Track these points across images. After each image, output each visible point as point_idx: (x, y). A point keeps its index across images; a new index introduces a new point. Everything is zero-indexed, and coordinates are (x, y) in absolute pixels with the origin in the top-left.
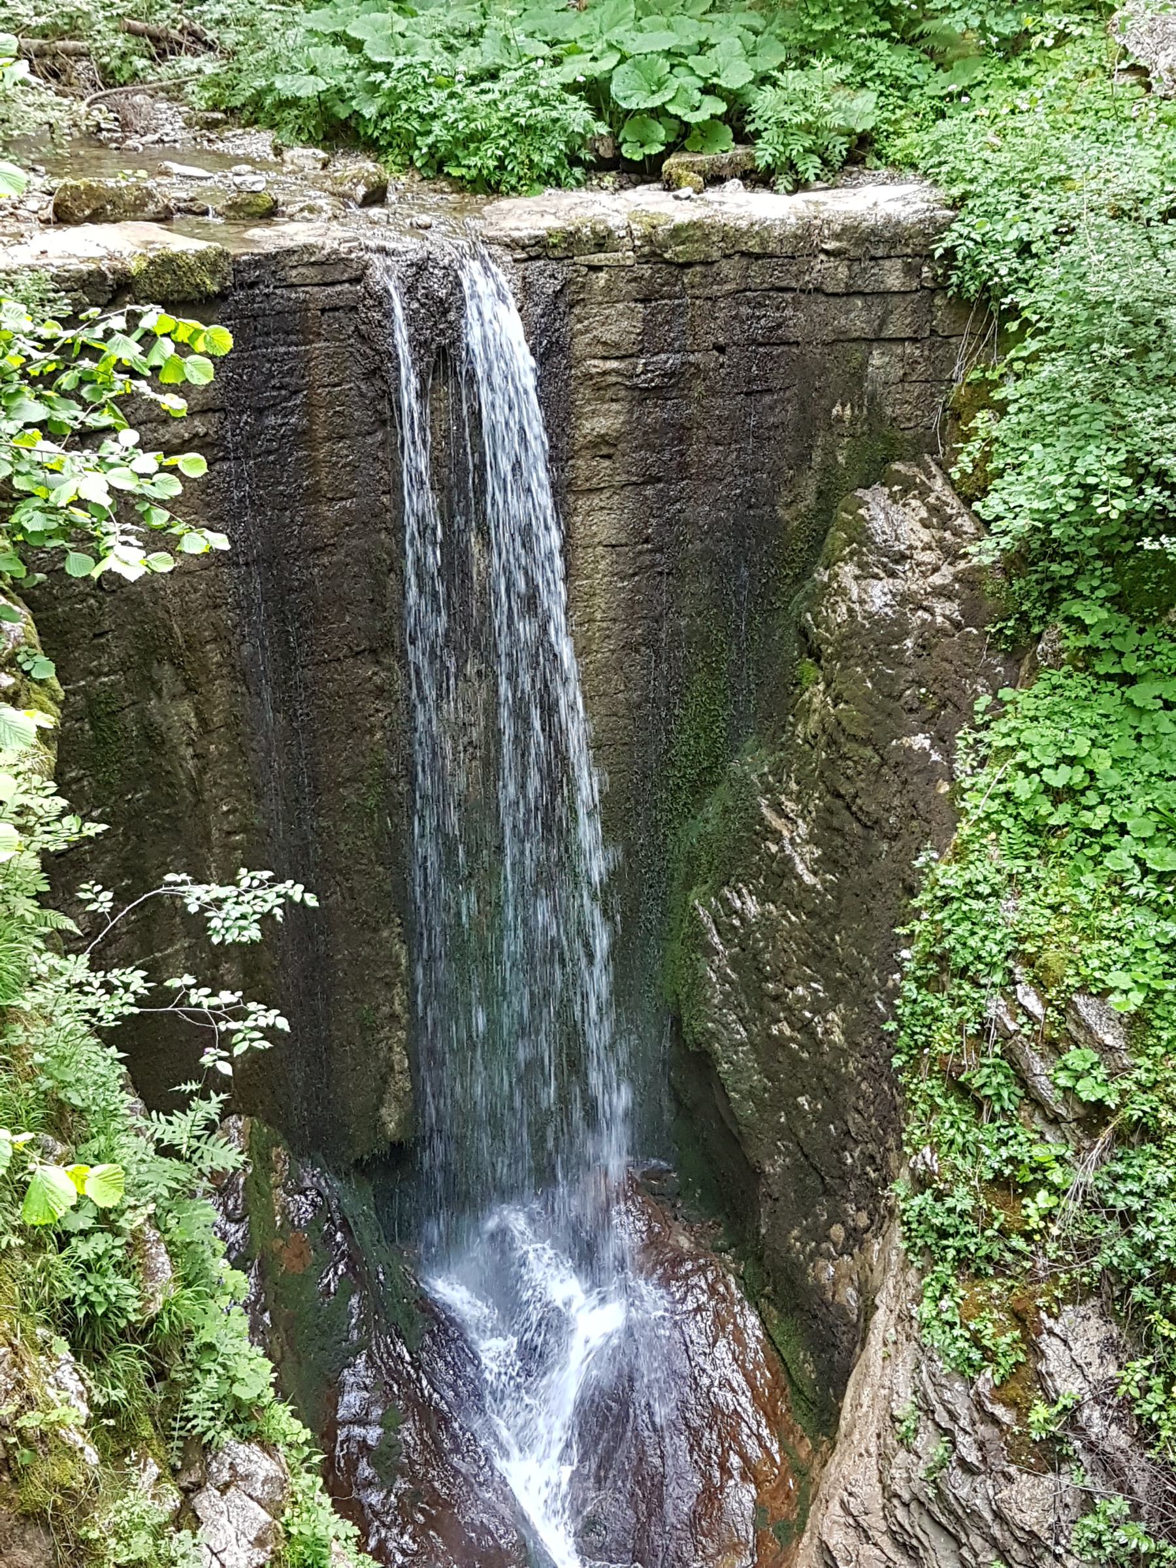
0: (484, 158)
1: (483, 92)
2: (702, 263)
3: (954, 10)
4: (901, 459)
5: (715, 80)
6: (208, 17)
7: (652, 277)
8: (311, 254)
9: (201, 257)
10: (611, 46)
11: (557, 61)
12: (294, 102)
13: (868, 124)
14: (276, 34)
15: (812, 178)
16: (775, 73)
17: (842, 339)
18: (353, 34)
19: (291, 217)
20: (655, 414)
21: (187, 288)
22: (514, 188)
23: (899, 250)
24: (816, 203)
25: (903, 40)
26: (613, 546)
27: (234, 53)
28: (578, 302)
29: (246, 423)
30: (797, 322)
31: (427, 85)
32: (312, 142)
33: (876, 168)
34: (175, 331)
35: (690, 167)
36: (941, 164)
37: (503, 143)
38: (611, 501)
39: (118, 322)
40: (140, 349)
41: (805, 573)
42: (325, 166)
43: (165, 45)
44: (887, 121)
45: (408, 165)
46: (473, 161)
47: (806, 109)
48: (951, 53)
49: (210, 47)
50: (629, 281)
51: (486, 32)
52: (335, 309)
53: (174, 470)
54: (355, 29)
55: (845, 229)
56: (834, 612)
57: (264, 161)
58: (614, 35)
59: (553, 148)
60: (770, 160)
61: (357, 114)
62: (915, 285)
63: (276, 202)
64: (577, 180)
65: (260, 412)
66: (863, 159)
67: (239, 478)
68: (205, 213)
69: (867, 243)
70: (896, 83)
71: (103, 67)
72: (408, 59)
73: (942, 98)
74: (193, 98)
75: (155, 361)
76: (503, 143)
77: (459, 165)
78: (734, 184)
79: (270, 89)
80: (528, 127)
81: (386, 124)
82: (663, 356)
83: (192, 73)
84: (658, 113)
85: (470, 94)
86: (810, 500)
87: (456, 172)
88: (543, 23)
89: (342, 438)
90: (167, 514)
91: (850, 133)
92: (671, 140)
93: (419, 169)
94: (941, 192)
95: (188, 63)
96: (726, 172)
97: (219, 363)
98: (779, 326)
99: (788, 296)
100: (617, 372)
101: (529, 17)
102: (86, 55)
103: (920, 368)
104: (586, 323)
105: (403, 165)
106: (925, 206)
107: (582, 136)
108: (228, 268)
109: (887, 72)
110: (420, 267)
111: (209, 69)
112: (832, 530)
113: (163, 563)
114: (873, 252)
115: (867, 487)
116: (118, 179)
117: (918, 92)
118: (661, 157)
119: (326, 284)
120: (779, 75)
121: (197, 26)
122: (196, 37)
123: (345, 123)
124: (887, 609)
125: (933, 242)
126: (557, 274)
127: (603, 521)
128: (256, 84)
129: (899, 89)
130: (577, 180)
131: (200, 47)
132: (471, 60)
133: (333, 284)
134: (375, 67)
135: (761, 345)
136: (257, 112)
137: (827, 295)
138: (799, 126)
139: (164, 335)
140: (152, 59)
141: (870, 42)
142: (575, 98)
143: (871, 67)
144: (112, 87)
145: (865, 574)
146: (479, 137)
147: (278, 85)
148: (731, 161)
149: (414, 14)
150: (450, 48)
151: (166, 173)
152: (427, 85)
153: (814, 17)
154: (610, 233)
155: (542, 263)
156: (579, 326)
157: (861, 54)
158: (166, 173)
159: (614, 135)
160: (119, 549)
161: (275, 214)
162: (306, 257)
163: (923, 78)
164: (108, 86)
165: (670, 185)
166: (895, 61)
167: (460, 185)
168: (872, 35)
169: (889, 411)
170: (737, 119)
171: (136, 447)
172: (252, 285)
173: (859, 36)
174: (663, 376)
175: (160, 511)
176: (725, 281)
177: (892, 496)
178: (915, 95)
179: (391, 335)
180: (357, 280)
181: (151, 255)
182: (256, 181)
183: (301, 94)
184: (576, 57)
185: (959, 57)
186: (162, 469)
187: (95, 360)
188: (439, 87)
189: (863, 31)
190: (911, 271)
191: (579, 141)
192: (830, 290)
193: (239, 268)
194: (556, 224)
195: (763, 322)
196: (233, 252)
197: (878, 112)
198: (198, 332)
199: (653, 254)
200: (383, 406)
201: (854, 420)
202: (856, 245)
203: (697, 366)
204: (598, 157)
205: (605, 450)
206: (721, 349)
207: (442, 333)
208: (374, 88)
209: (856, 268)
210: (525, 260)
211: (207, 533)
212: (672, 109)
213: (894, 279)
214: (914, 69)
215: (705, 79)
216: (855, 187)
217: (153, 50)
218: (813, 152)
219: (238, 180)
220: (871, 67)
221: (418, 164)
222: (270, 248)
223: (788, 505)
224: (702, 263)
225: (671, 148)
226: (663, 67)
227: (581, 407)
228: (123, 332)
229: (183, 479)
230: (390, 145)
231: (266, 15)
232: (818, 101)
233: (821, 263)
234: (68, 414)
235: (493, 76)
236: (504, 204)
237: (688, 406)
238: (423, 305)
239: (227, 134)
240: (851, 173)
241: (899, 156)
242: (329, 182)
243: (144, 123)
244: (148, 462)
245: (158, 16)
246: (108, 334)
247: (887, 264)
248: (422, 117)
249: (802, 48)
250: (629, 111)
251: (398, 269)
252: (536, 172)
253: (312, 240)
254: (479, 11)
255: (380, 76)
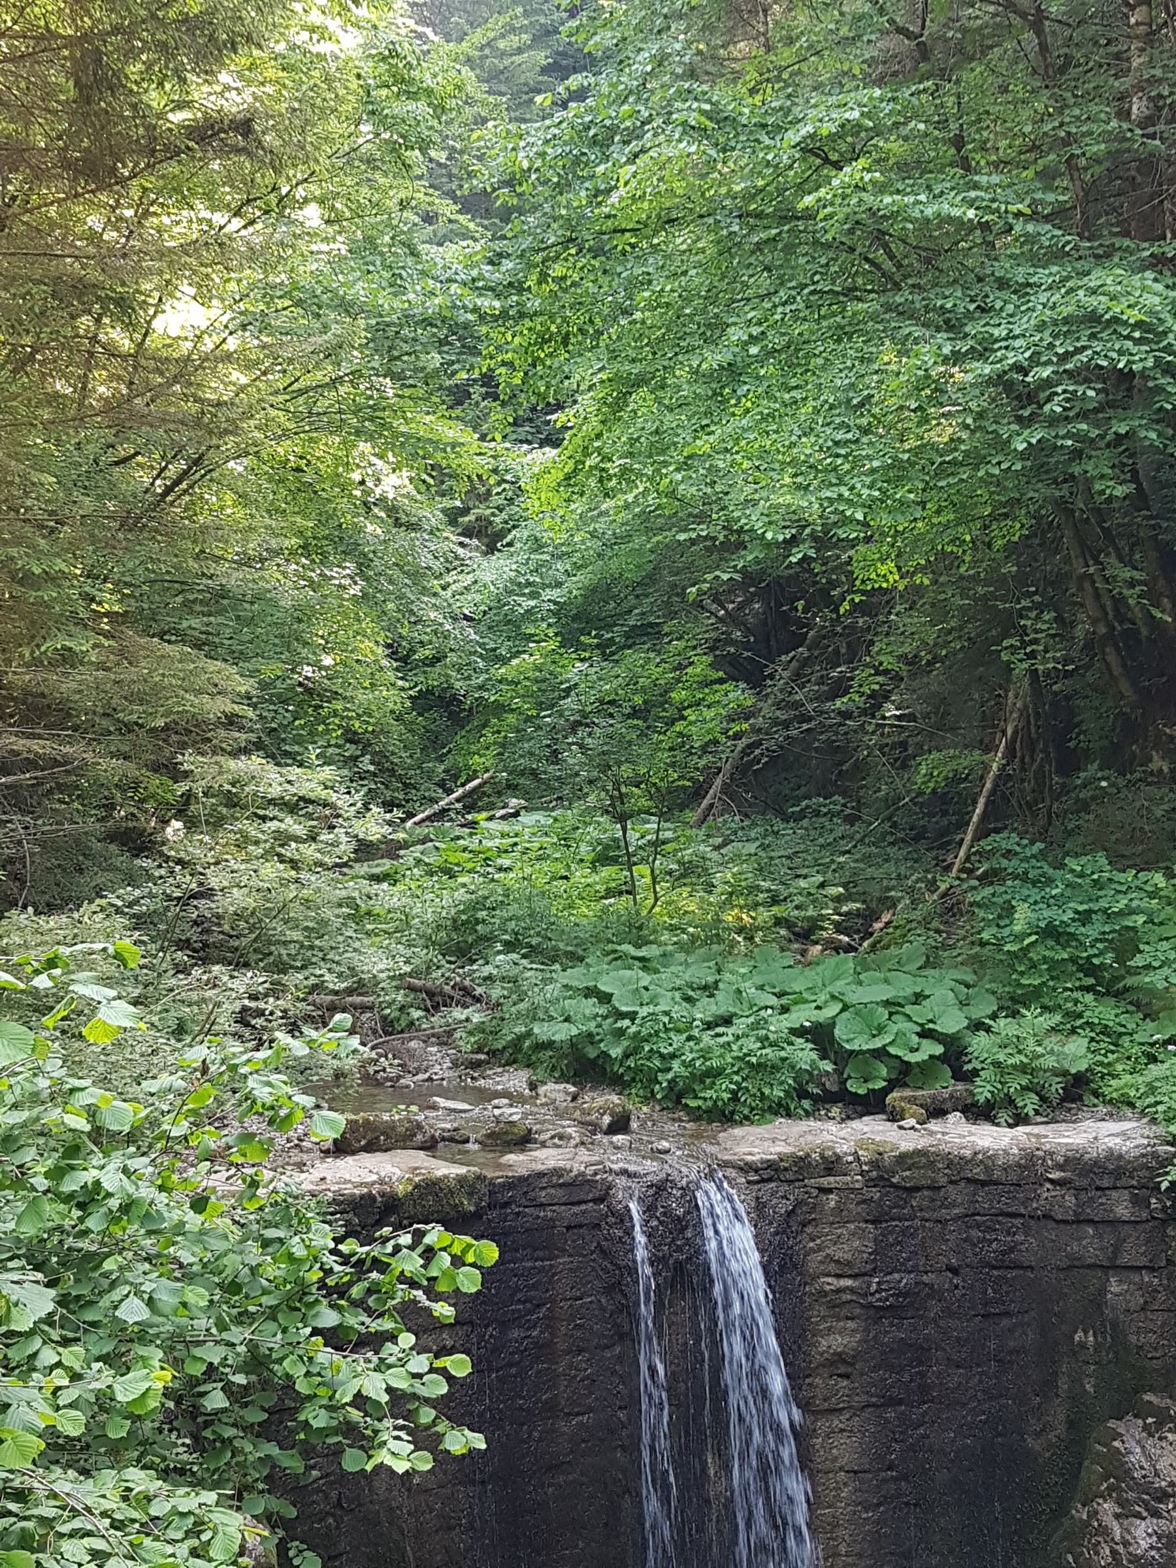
0: (721, 1091)
1: (718, 1035)
2: (929, 1188)
3: (1155, 968)
4: (1152, 1389)
5: (931, 1026)
6: (477, 975)
7: (881, 1199)
8: (561, 1176)
9: (461, 1180)
10: (833, 997)
11: (785, 1010)
12: (550, 1045)
13: (1083, 1066)
14: (536, 989)
15: (1031, 1113)
16: (987, 1021)
17: (1075, 1265)
18: (603, 988)
19: (543, 1145)
20: (892, 1334)
21: (447, 1209)
22: (747, 1118)
23: (1124, 1181)
24: (1037, 1136)
25: (1108, 993)
26: (855, 1472)
27: (499, 1004)
28: (810, 1222)
29: (491, 1336)
30: (1029, 1246)
31: (667, 1030)
32: (563, 1078)
33: (1095, 1106)
34: (450, 1246)
35: (912, 1100)
36: (1158, 1103)
37: (736, 1078)
38: (850, 1423)
39: (406, 1239)
40: (422, 1262)
41: (1061, 1512)
42: (574, 1099)
43: (440, 999)
44: (1101, 1064)
45: (650, 1098)
46: (708, 1094)
47: (1020, 1052)
48: (1157, 1004)
49: (478, 1000)
50: (858, 1204)
51: (721, 985)
52: (581, 1226)
53: (443, 1372)
54: (605, 984)
55: (1067, 1160)
56: (1097, 1553)
57: (521, 1095)
58: (838, 987)
59: (782, 1083)
60: (989, 1096)
61: (604, 1054)
62: (1145, 1215)
63: (530, 1131)
64: (806, 1111)
65: (504, 1326)
66: (1080, 1098)
67: (481, 1390)
68: (467, 1141)
69: (1092, 1174)
70: (1105, 1031)
71: (384, 1018)
72: (651, 1008)
73: (1152, 1045)
74: (461, 1043)
75: (434, 1273)
76: (736, 1078)
77: (696, 1097)
78: (955, 1117)
79: (529, 1034)
80: (759, 1065)
81: (631, 1063)
82: (896, 1276)
83: (461, 1022)
84: (881, 1054)
85: (707, 1039)
86: (1061, 1429)
87: (693, 1103)
88: (772, 978)
89: (580, 1351)
90: (433, 1413)
91: (1065, 1073)
92: (893, 1077)
93: (659, 1101)
94: (1160, 1130)
95: (459, 1014)
96: (949, 1105)
97: (488, 1274)
98: (1011, 1250)
99: (1018, 1222)
100: (851, 1290)
101: (760, 973)
102: (371, 1008)
103: (1162, 1297)
104: (818, 1241)
105: (645, 1097)
106: (1146, 1142)
107: (810, 1073)
108: (484, 1190)
109: (1096, 1021)
110: (660, 1188)
111: (476, 1019)
112: (1086, 1463)
113: (424, 1462)
114: (1098, 1183)
115: (1120, 1419)
116: (394, 1115)
117: (1127, 1039)
118: (885, 1091)
119: (573, 1204)
120: (991, 1023)
121: (467, 983)
122: (467, 991)
123: (593, 1062)
124: (1153, 1553)
125: (1159, 1175)
126: (788, 1198)
127: (843, 1446)
128: (516, 1030)
129: (1109, 1036)
130: (806, 1111)
131: (468, 1000)
132: (706, 1009)
133: (579, 1203)
134: (622, 1015)
135: (994, 1268)
136: (516, 1054)
137: (1058, 1222)
138: (1014, 1067)
139: (441, 1249)
140: (427, 1010)
141: (1077, 995)
142: (802, 1040)
143: (1080, 1016)
144: (391, 1034)
145: (1126, 1514)
146: (715, 1073)
147: (536, 1030)
148: (952, 1096)
149: (657, 971)
150: (688, 999)
151: (434, 1107)
152: (667, 1030)
153: (1022, 974)
154: (839, 1158)
155: (773, 1185)
156: (811, 1245)
157: (1069, 1005)
158: (434, 1107)
159: (839, 1072)
160: (393, 1445)
161: (528, 1141)
162: (555, 1179)
163: (1131, 1026)
164: (387, 1033)
165: (895, 1116)
166: (1106, 1012)
167: (696, 1115)
168: (1077, 989)
169: (1133, 1339)
170: (954, 1056)
171: (412, 1349)
172: (506, 1205)
173: (1066, 989)
174: (898, 1295)
175: (427, 1409)
176: (954, 1205)
177: (1146, 1428)
178: (1125, 1041)
179: (632, 1250)
180: (601, 1200)
181: (417, 1179)
182: (514, 1113)
183: (557, 1038)
184: (802, 1006)
185: (1164, 1008)
186: (432, 1370)
187: (382, 1272)
188: (679, 1031)
189: (1069, 985)
190: (1139, 1202)
191: (807, 1077)
192: (1060, 1217)
193: (494, 1189)
194: (788, 1150)
195: (994, 1245)
196: (490, 1175)
197: (1090, 1056)
198: (469, 1246)
199: (881, 1178)
200: (622, 1319)
201: (1098, 1347)
202: (1079, 1175)
203: (931, 1286)
204: (825, 1090)
205: (842, 1369)
206: (955, 1271)
207: (679, 1249)
208: (621, 1032)
209: (1083, 1197)
210: (758, 1182)
211: (466, 1432)
212: (892, 1050)
213: (1123, 1210)
214: (1122, 1019)
215: (922, 1025)
216: (1074, 1122)
217: (429, 1003)
218: (1030, 1090)
219: (497, 1112)
220: (1080, 1016)
221: (659, 1096)
222: (523, 1172)
223: (1038, 1434)
224: (929, 1188)
225: (892, 1085)
226: (882, 1015)
227: (817, 1324)
228: (409, 1248)
229: (450, 1378)
230: (633, 1080)
231: (529, 974)
232: (1031, 1045)
233: (1046, 1192)
234: (356, 1320)
235: (727, 1021)
236: (738, 1131)
237: (925, 1327)
238: (661, 1223)
239: (489, 1072)
240: (1070, 1109)
241: (1115, 1095)
242: (578, 1112)
243: (416, 1065)
244: (419, 1363)
245: (434, 975)
246: (397, 1249)
247: (1114, 1194)
248: (662, 1056)
249: (1012, 999)
250: (852, 1052)
251: (637, 1188)
252: (767, 1103)
253: (561, 1164)
254: (714, 968)
255: (627, 1022)
